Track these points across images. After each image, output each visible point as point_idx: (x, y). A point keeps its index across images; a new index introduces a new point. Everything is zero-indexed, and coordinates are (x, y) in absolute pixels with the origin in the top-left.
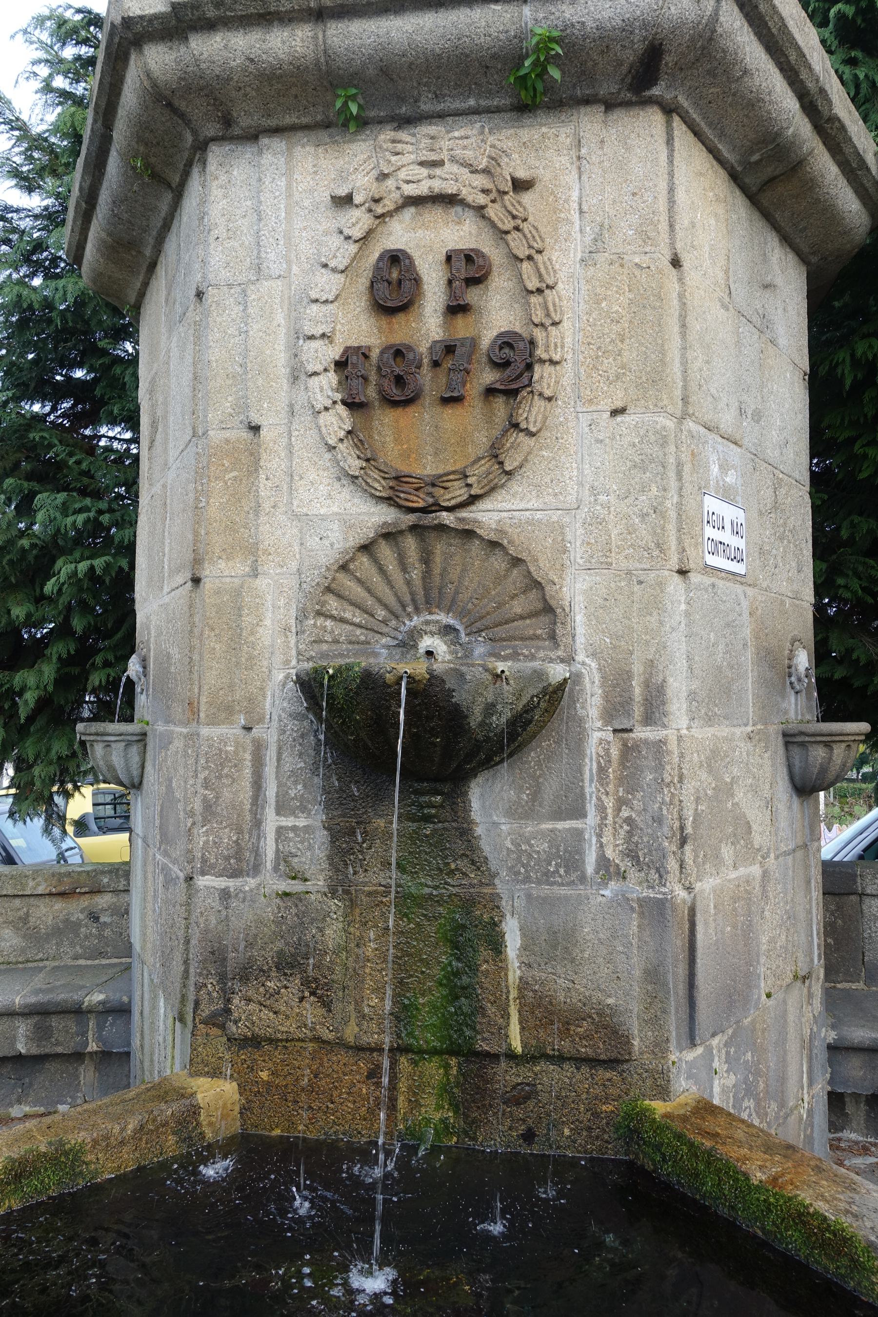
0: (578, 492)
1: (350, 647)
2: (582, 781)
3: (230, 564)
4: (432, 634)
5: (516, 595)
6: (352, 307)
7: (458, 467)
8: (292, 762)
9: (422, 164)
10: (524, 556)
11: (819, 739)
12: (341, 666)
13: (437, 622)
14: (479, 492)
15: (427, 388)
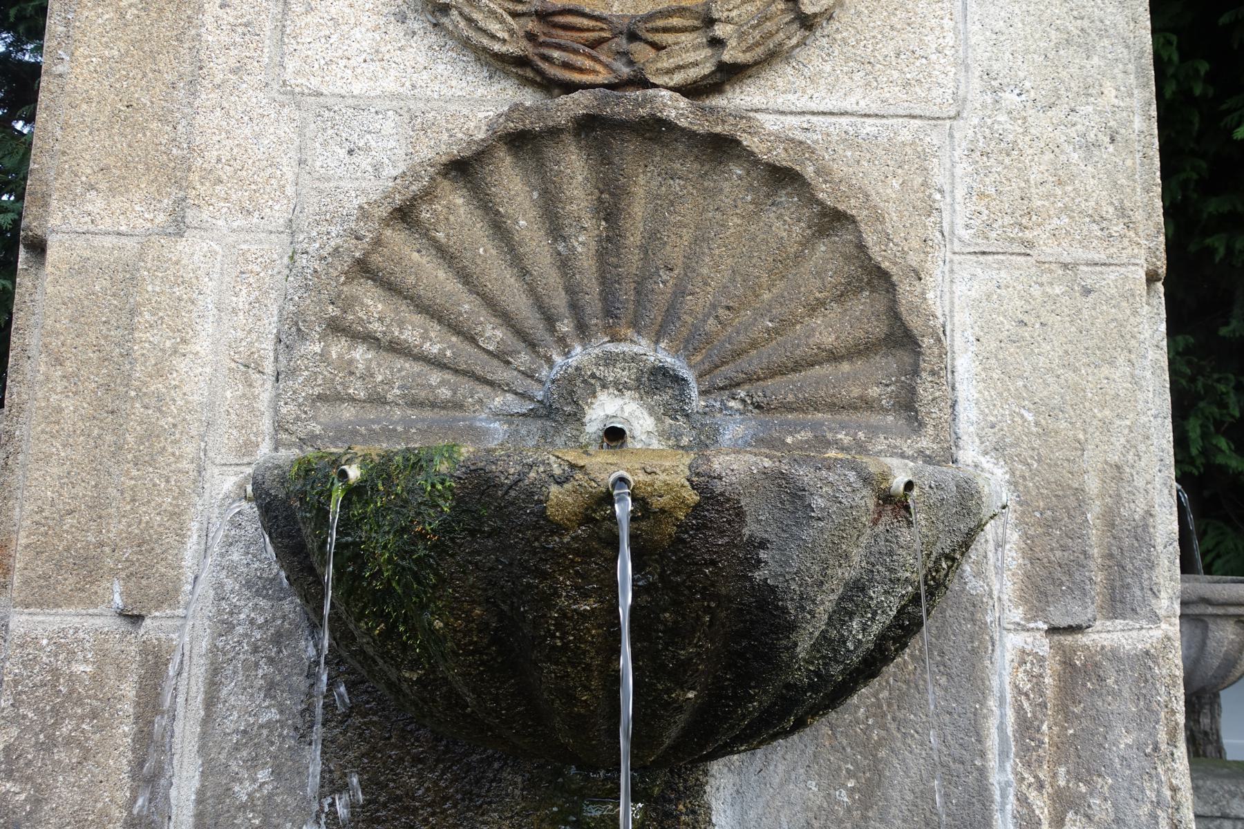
0: (957, 81)
1: (413, 414)
2: (983, 755)
3: (117, 202)
4: (620, 388)
5: (822, 303)
8: (245, 707)
10: (849, 206)
11: (1232, 610)
12: (388, 458)
13: (635, 358)
14: (742, 58)
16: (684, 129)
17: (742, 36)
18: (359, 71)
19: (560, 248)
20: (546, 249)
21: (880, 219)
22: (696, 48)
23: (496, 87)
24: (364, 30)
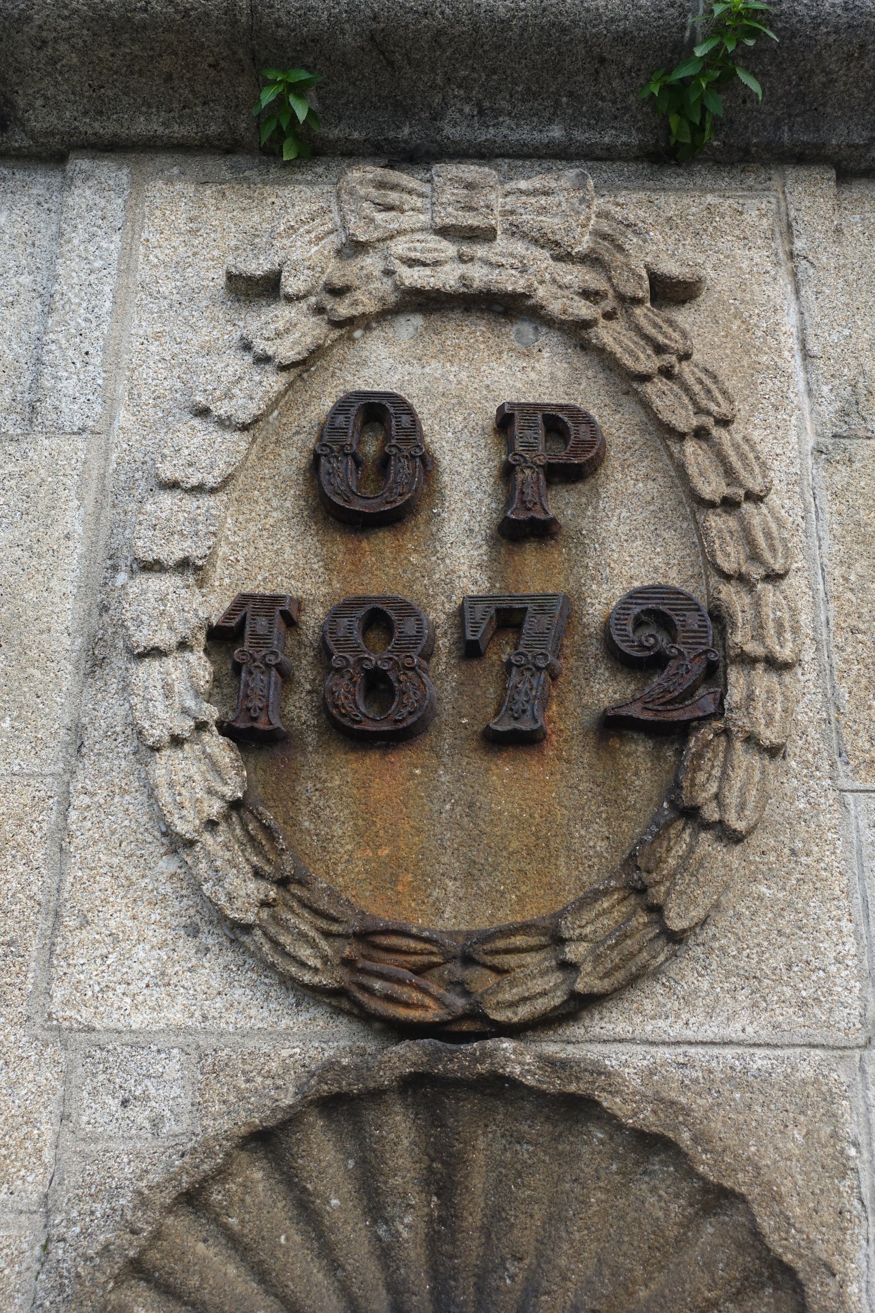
6: (261, 508)
7: (530, 914)
9: (444, 232)
10: (740, 1182)
15: (446, 708)
16: (532, 1087)
17: (598, 959)
18: (140, 998)
19: (381, 1232)
20: (364, 1233)
21: (777, 1198)
22: (543, 974)
23: (304, 1017)
24: (147, 947)
